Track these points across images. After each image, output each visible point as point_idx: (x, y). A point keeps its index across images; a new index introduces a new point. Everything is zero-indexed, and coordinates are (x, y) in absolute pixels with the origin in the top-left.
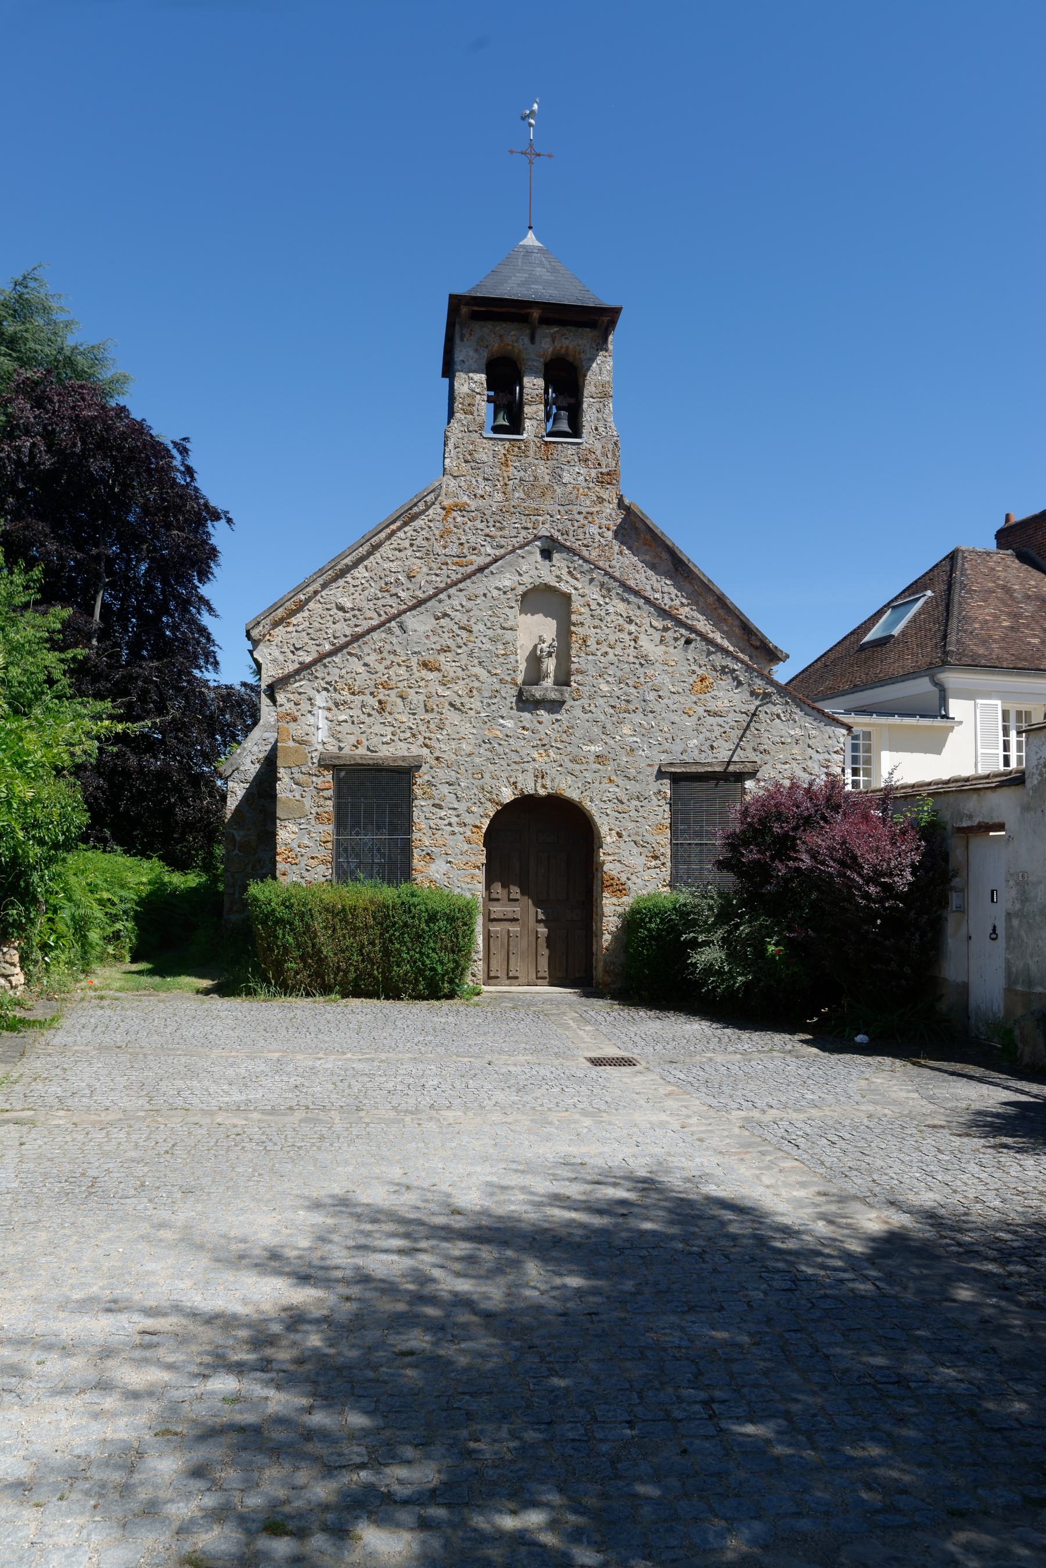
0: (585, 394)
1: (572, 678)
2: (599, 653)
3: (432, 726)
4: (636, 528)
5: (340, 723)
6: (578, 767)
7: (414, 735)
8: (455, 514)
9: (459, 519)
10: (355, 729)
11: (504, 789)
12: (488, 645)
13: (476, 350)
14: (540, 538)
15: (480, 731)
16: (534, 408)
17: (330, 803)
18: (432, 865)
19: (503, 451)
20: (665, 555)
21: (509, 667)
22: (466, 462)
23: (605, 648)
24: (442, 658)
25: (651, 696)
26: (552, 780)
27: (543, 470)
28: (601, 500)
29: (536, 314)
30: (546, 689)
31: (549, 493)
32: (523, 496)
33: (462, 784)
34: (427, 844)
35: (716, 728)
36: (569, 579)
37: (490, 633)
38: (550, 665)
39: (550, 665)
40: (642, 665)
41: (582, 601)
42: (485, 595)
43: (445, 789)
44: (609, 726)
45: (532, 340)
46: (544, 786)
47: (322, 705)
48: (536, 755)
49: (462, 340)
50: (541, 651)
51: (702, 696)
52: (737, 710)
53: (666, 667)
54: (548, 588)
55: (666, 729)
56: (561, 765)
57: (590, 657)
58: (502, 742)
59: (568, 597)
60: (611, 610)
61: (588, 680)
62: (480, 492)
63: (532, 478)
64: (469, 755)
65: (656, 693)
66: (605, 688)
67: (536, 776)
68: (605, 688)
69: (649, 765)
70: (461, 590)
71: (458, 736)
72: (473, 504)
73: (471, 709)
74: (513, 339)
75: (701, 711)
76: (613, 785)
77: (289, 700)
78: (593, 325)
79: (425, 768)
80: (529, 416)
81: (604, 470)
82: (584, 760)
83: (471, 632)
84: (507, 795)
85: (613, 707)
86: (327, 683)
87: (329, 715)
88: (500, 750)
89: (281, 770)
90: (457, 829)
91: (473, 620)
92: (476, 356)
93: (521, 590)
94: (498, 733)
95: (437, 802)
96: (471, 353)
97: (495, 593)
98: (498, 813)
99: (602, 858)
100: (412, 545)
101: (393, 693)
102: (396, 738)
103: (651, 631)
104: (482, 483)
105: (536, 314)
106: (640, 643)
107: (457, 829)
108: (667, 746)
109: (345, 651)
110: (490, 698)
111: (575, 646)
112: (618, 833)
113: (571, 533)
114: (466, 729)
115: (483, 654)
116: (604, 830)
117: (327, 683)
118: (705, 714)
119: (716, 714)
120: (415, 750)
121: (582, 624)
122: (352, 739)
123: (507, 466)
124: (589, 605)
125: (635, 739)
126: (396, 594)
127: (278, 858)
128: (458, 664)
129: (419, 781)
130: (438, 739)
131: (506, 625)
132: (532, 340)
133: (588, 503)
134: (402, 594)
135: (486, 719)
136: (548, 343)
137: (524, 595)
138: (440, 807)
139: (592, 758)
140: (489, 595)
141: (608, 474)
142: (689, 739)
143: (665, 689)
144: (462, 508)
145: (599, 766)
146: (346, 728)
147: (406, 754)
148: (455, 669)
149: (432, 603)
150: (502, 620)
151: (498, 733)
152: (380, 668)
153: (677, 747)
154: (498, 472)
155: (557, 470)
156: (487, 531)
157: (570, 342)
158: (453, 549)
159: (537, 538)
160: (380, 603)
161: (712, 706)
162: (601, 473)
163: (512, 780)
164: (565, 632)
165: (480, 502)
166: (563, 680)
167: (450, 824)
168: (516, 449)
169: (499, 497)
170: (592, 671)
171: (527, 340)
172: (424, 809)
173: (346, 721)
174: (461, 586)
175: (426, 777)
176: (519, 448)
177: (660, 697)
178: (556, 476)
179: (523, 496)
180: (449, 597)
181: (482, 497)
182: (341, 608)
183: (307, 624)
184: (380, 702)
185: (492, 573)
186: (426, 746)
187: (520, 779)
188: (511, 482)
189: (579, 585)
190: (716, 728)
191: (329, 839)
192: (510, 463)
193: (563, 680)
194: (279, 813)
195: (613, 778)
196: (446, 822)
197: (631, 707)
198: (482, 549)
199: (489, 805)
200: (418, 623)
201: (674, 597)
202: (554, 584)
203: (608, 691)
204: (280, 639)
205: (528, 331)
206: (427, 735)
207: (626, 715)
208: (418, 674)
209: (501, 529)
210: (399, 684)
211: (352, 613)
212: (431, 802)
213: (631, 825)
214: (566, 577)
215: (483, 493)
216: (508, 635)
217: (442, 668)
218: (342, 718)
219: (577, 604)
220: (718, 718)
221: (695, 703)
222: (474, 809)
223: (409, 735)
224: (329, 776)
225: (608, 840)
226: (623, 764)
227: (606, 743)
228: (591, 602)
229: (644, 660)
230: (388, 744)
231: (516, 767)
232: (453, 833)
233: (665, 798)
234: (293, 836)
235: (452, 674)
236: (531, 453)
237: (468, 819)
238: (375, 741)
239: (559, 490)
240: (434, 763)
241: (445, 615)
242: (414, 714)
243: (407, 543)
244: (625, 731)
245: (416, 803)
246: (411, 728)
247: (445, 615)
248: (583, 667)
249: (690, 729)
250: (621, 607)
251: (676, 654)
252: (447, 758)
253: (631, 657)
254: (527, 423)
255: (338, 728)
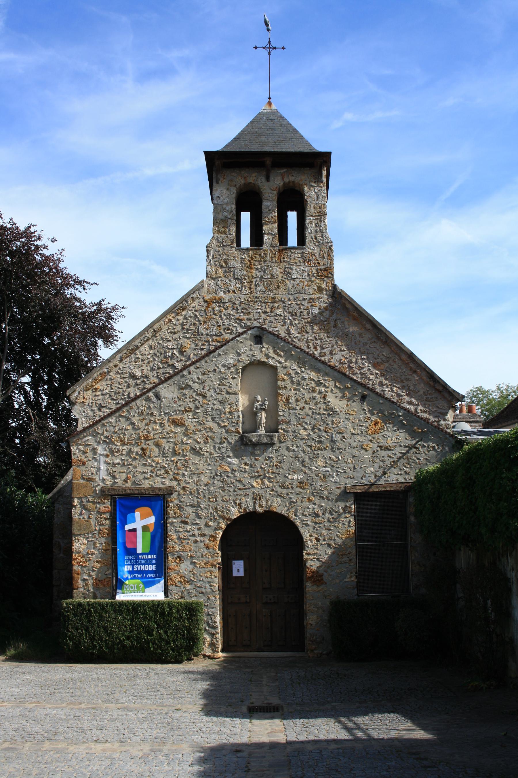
0: (307, 215)
1: (280, 427)
2: (298, 408)
3: (179, 465)
4: (347, 309)
5: (114, 465)
6: (285, 491)
7: (167, 472)
8: (214, 305)
9: (217, 309)
10: (124, 469)
11: (232, 508)
12: (218, 406)
13: (228, 189)
14: (253, 328)
15: (214, 468)
16: (270, 226)
17: (108, 522)
18: (182, 565)
19: (248, 259)
20: (368, 326)
21: (234, 420)
22: (222, 267)
23: (301, 404)
24: (185, 416)
25: (337, 437)
26: (267, 501)
27: (277, 270)
28: (320, 290)
29: (268, 161)
30: (260, 436)
31: (282, 286)
32: (263, 289)
33: (202, 506)
34: (178, 550)
35: (386, 459)
36: (275, 356)
37: (220, 397)
38: (263, 417)
39: (263, 417)
40: (329, 415)
41: (285, 371)
42: (215, 370)
43: (190, 510)
44: (307, 460)
45: (268, 179)
46: (261, 506)
47: (102, 453)
48: (255, 484)
49: (217, 183)
50: (256, 409)
51: (376, 436)
52: (402, 444)
53: (348, 416)
54: (260, 363)
55: (350, 461)
56: (273, 490)
57: (291, 411)
58: (230, 475)
59: (275, 368)
60: (306, 376)
61: (291, 428)
62: (232, 288)
63: (269, 276)
64: (206, 485)
65: (341, 435)
66: (303, 432)
67: (255, 499)
68: (303, 432)
69: (338, 488)
70: (198, 368)
71: (198, 472)
72: (226, 297)
73: (207, 452)
74: (255, 178)
75: (374, 446)
76: (311, 503)
77: (80, 450)
78: (311, 166)
79: (174, 496)
80: (267, 232)
81: (322, 267)
82: (289, 486)
83: (206, 397)
84: (235, 512)
85: (310, 446)
86: (106, 437)
87: (108, 460)
88: (228, 480)
89: (76, 500)
90: (199, 539)
91: (207, 388)
92: (228, 193)
93: (240, 366)
94: (227, 468)
95: (184, 519)
96: (225, 191)
97: (222, 369)
98: (228, 526)
99: (305, 557)
100: (183, 328)
101: (151, 442)
102: (153, 475)
103: (335, 390)
104: (234, 282)
105: (268, 161)
106: (328, 399)
107: (199, 539)
108: (350, 473)
109: (117, 414)
110: (220, 443)
111: (281, 403)
112: (316, 538)
113: (298, 315)
114: (203, 466)
115: (214, 412)
116: (306, 536)
117: (106, 437)
118: (378, 449)
119: (387, 449)
120: (168, 483)
121: (285, 388)
122: (124, 476)
123: (251, 268)
124: (290, 374)
125: (327, 469)
126: (173, 365)
127: (74, 563)
128: (197, 420)
129: (171, 505)
130: (184, 474)
131: (231, 391)
132: (268, 179)
133: (311, 291)
134: (176, 364)
135: (218, 459)
136: (278, 180)
137: (244, 369)
138: (186, 523)
139: (295, 484)
140: (218, 370)
141: (325, 270)
142: (367, 467)
143: (348, 432)
144: (220, 301)
145: (301, 490)
146: (118, 469)
147: (161, 486)
148: (195, 424)
149: (177, 378)
150: (227, 388)
151: (227, 468)
152: (142, 425)
153: (358, 474)
154: (245, 273)
155: (287, 270)
156: (237, 316)
157: (295, 177)
158: (214, 330)
159: (250, 328)
160: (160, 371)
161: (382, 442)
162: (321, 270)
163: (238, 502)
164: (275, 392)
165: (232, 296)
166: (273, 429)
167: (194, 535)
168: (257, 256)
169: (246, 291)
170: (294, 421)
171: (264, 179)
172: (175, 525)
173: (119, 464)
174: (198, 365)
175: (176, 502)
176: (260, 255)
177: (344, 438)
178: (288, 274)
179: (263, 289)
180: (190, 373)
181: (234, 292)
182: (133, 377)
183: (109, 388)
184: (142, 449)
185: (219, 355)
186: (176, 479)
187: (244, 500)
188: (255, 280)
189: (282, 360)
190: (386, 459)
191: (108, 548)
192: (253, 267)
193: (273, 429)
194: (75, 530)
195: (312, 498)
196: (191, 534)
197: (323, 446)
198: (234, 329)
199: (221, 521)
200: (168, 392)
201: (376, 356)
202: (264, 359)
203: (306, 435)
204: (91, 401)
205: (264, 173)
206: (176, 471)
207: (319, 452)
208: (169, 428)
209: (248, 314)
210: (156, 436)
211: (142, 379)
212: (179, 520)
213: (325, 532)
214: (272, 354)
215: (234, 289)
216: (232, 398)
217: (186, 423)
218: (117, 461)
219: (281, 373)
220: (388, 452)
221: (371, 441)
222: (211, 524)
223: (163, 472)
224: (108, 503)
225: (309, 543)
226: (318, 487)
227: (305, 473)
228: (292, 372)
229: (332, 412)
230: (148, 478)
231: (241, 492)
232: (196, 542)
233: (350, 512)
234: (84, 546)
235: (192, 428)
236: (268, 259)
237: (207, 531)
238: (140, 477)
239: (289, 284)
240: (181, 492)
241: (188, 386)
242: (166, 457)
243: (179, 328)
244: (319, 464)
245: (170, 520)
246: (164, 467)
247: (188, 386)
248: (287, 419)
249: (368, 461)
250: (313, 375)
251: (356, 406)
252: (191, 487)
253: (322, 410)
254: (266, 237)
255: (114, 469)
